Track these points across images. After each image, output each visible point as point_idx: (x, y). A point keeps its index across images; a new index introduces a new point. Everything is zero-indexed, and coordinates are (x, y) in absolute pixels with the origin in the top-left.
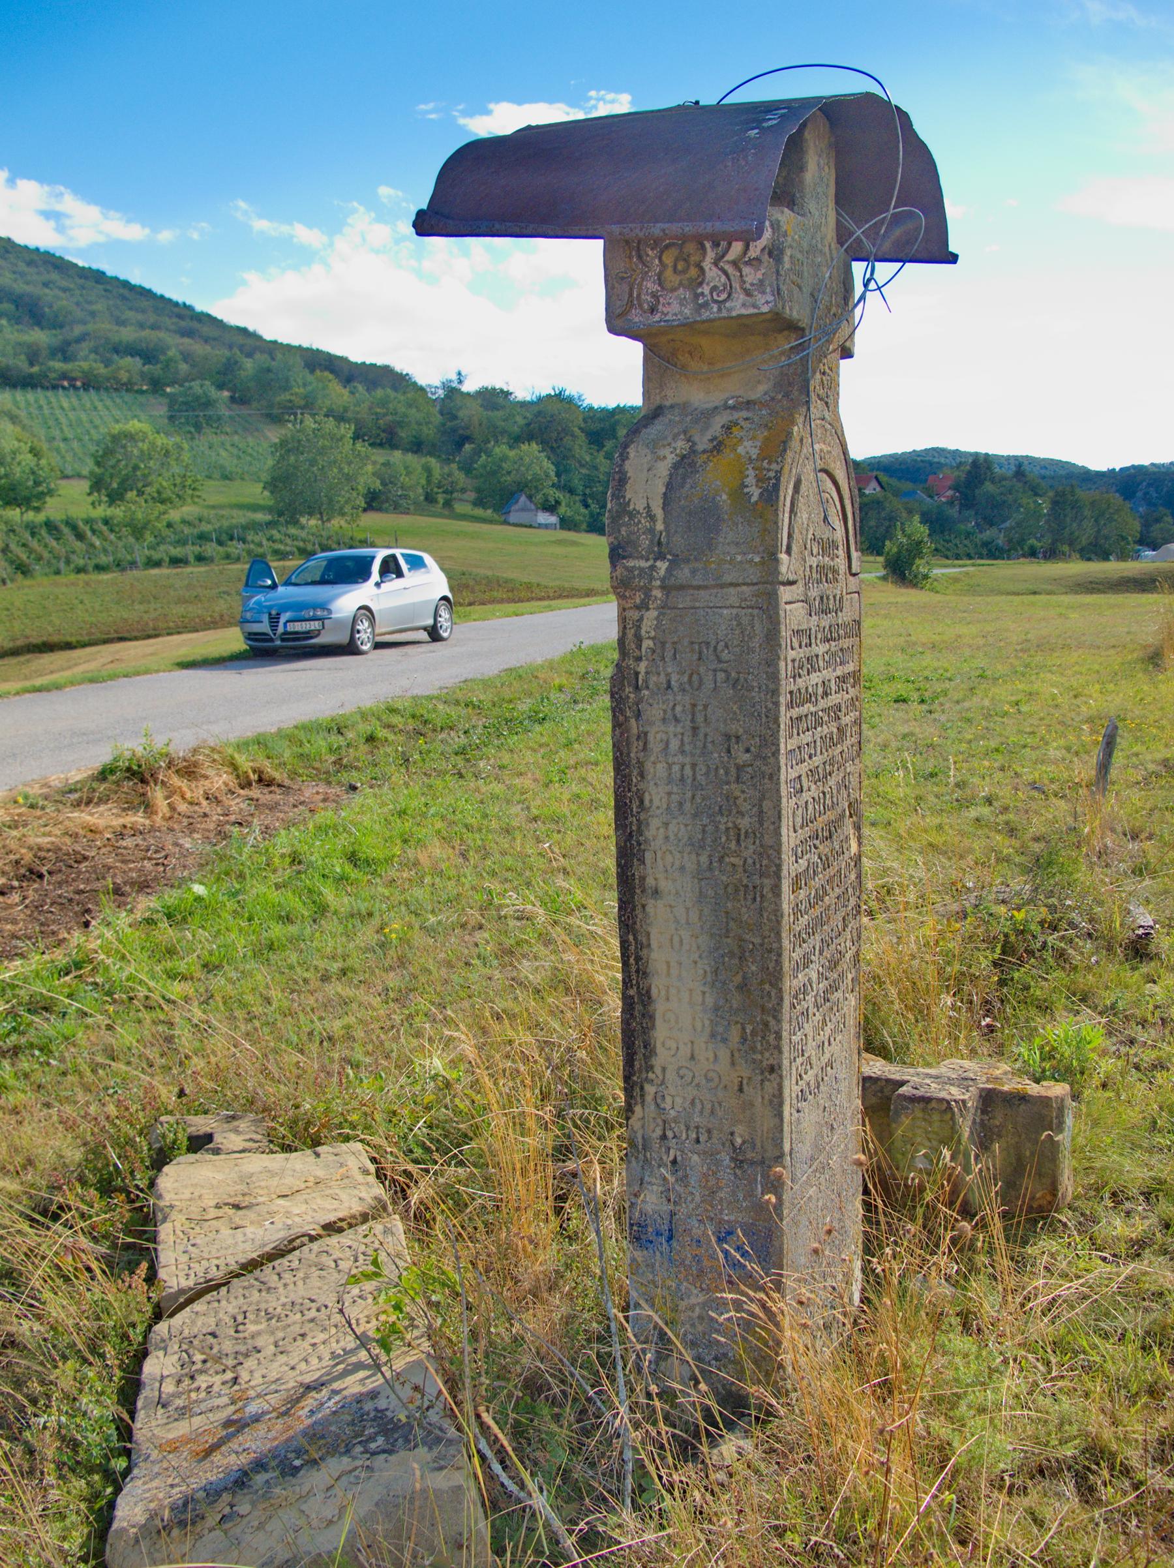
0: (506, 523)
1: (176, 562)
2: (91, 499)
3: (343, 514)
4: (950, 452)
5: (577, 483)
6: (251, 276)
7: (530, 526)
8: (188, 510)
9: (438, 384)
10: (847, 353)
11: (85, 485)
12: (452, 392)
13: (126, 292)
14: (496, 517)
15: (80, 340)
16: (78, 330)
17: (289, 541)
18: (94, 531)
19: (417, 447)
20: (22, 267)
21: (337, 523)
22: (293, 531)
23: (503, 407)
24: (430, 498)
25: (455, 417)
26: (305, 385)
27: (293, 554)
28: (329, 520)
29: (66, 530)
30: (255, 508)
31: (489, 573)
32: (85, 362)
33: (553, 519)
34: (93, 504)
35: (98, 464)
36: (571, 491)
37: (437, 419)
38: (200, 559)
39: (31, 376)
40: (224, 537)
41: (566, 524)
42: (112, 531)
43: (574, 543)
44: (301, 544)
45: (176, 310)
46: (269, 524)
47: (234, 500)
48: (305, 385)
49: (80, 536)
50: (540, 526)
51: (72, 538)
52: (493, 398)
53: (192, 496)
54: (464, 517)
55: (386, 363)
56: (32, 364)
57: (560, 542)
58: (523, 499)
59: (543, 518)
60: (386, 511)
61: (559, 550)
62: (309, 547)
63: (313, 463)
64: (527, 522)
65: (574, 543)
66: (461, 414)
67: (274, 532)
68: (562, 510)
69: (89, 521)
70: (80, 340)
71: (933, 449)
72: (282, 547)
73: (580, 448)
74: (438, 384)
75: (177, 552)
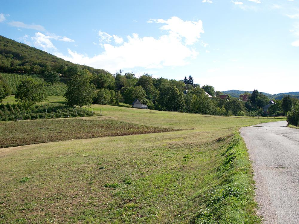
0: (133, 107)
1: (33, 118)
2: (16, 99)
3: (86, 104)
4: (237, 91)
5: (151, 97)
6: (76, 53)
7: (140, 108)
8: (44, 103)
9: (115, 74)
10: (189, 81)
11: (14, 96)
12: (118, 75)
13: (41, 53)
14: (130, 106)
15: (27, 62)
16: (27, 60)
17: (69, 112)
18: (14, 108)
19: (109, 88)
20: (16, 46)
21: (84, 107)
22: (71, 109)
23: (132, 78)
24: (112, 101)
25: (119, 80)
26: (81, 72)
27: (69, 116)
28: (82, 106)
29: (6, 108)
30: (63, 103)
31: (129, 122)
32: (28, 67)
33: (146, 106)
34: (16, 101)
35: (18, 90)
36: (150, 99)
37: (114, 81)
38: (41, 117)
39: (11, 69)
40: (50, 110)
41: (149, 108)
42: (19, 108)
43: (153, 113)
44: (72, 113)
45: (52, 57)
46: (65, 107)
47: (58, 101)
48: (81, 72)
49: (10, 110)
50: (142, 108)
51: (7, 110)
52: (129, 76)
53: (45, 99)
54: (121, 106)
55: (103, 69)
56: (12, 67)
57: (149, 112)
58: (138, 101)
59: (143, 106)
60: (100, 104)
61: (150, 115)
62: (75, 114)
63: (78, 89)
64: (139, 107)
65: (153, 113)
66: (121, 80)
67: (65, 109)
68: (148, 104)
69: (14, 106)
70: (27, 62)
71: (233, 90)
72: (66, 113)
73: (152, 88)
74: (115, 74)
75: (33, 114)
